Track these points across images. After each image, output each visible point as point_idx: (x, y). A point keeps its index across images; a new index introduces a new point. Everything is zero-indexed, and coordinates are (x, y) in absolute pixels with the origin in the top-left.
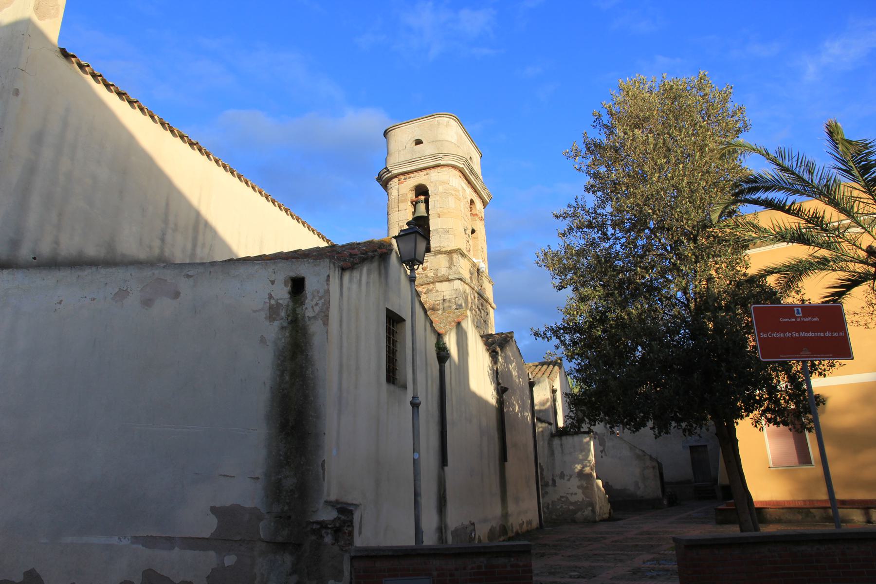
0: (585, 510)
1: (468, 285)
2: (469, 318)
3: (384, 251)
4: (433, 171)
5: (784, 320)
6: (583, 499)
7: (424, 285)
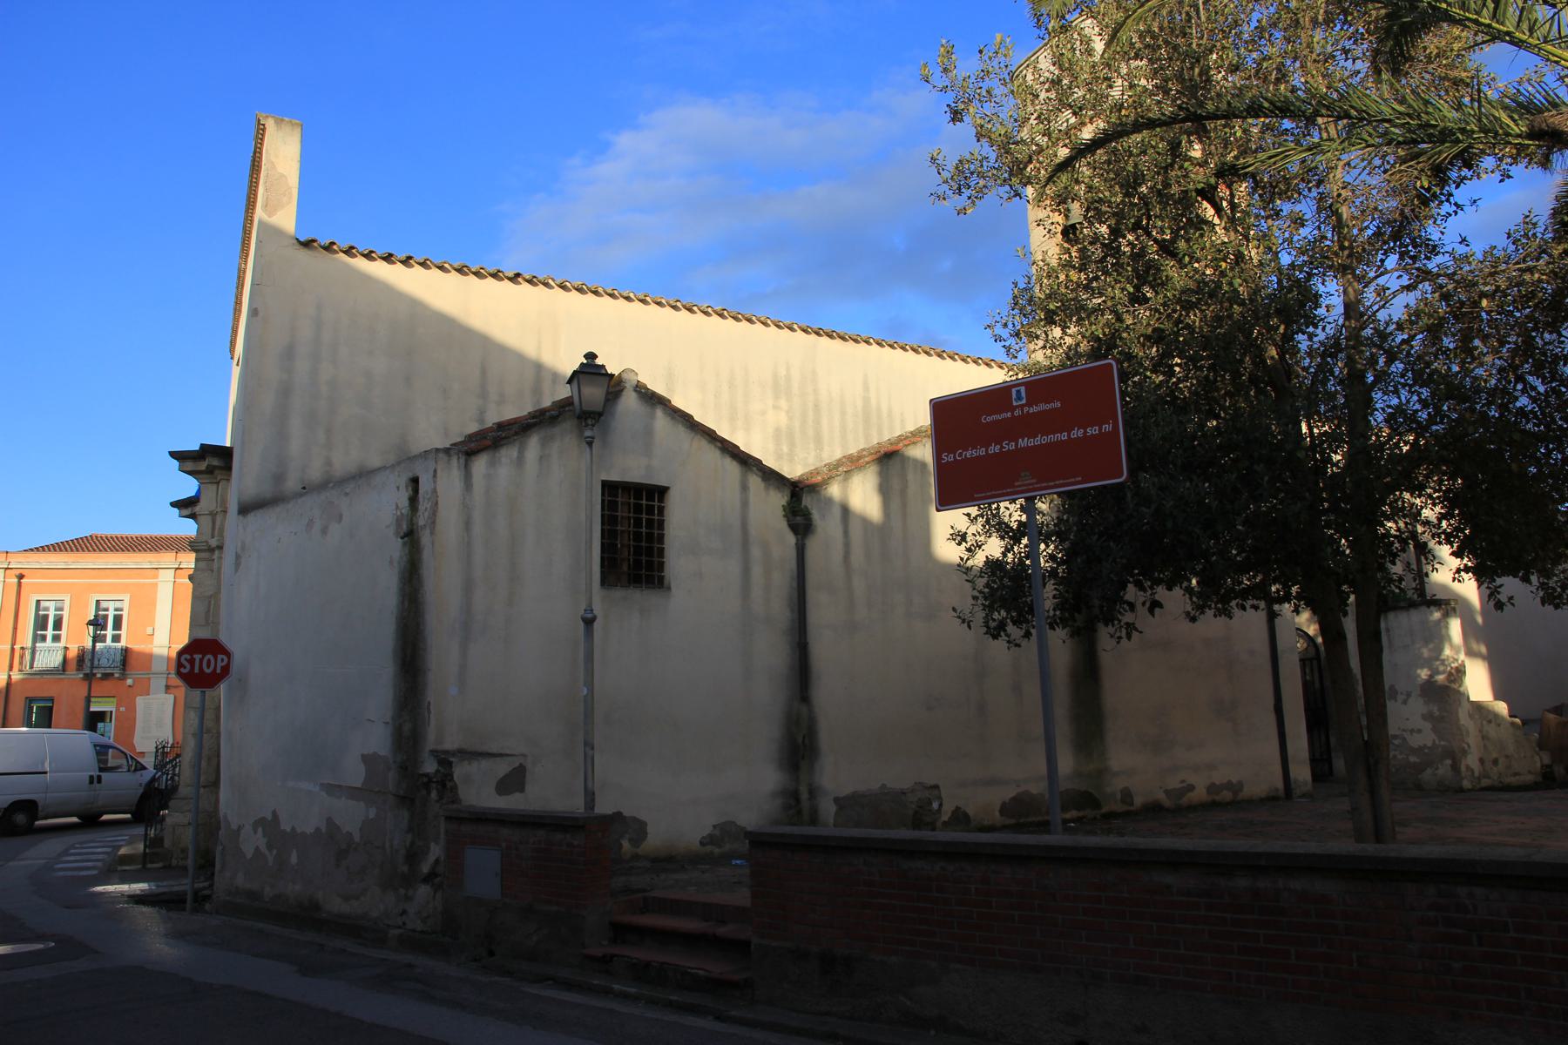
0: (1439, 766)
5: (990, 419)
6: (1434, 741)
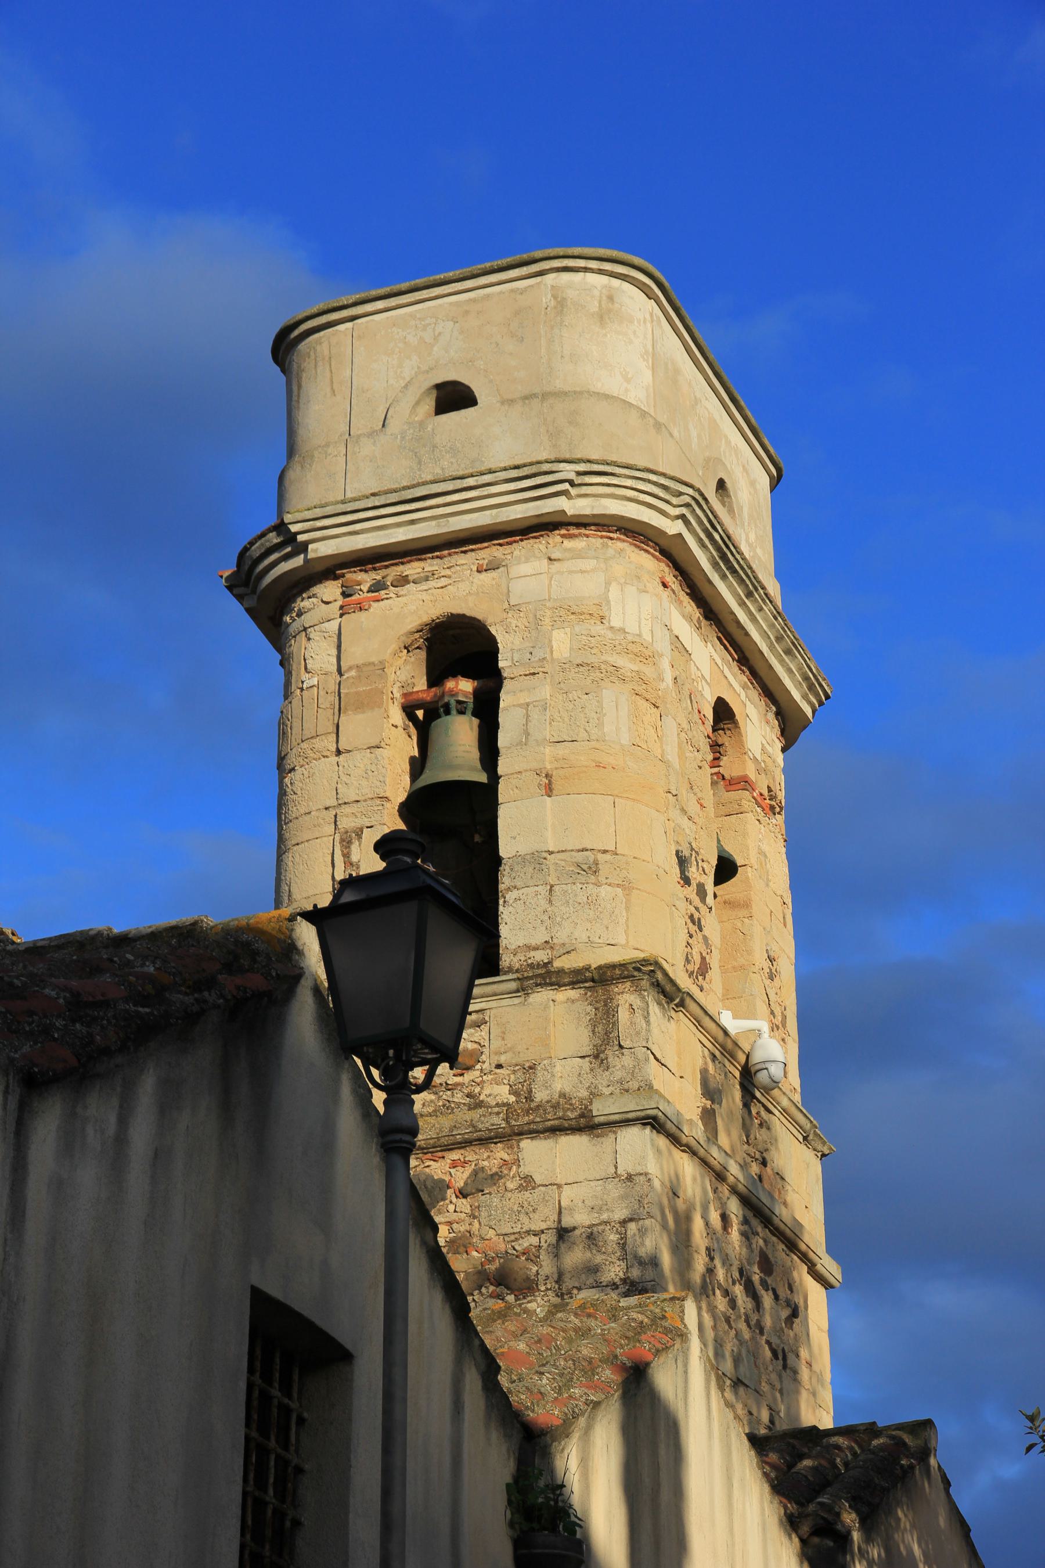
1: (694, 1153)
2: (695, 1344)
3: (255, 981)
4: (521, 549)
7: (466, 1144)
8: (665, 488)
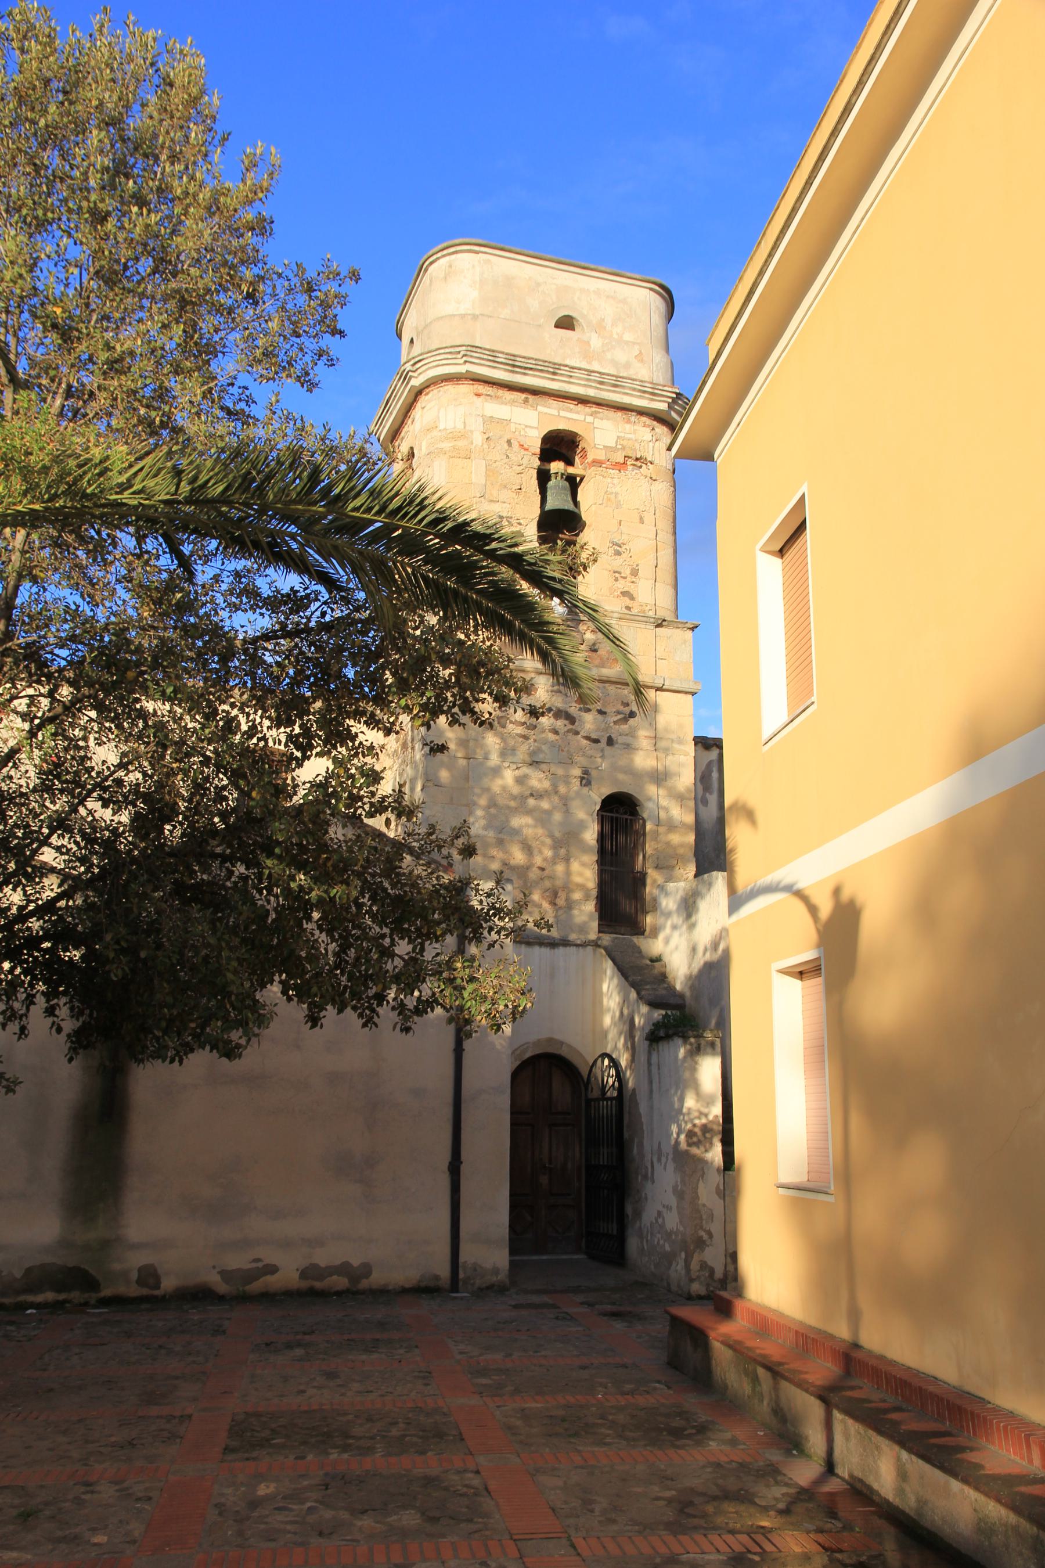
8: (450, 353)
